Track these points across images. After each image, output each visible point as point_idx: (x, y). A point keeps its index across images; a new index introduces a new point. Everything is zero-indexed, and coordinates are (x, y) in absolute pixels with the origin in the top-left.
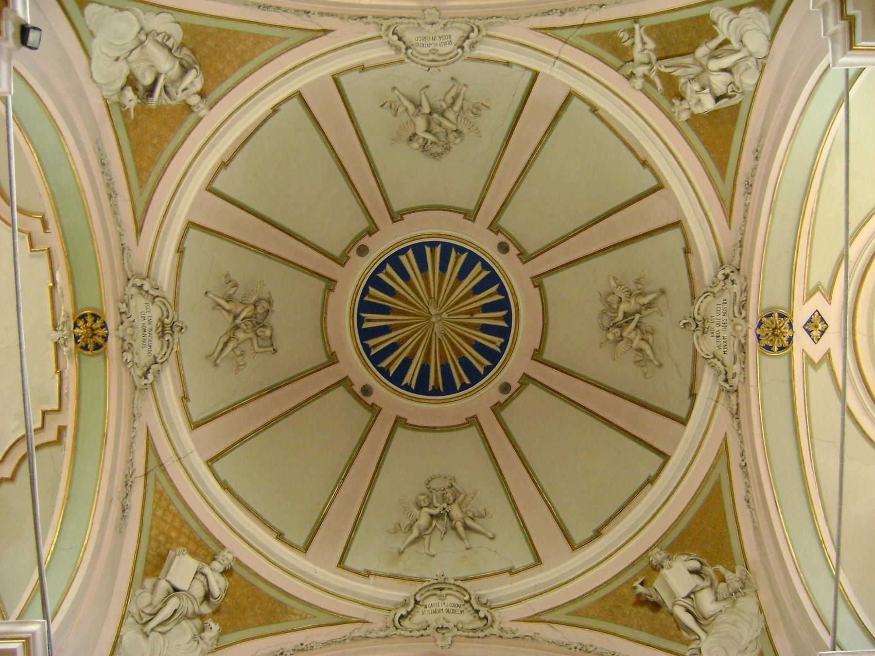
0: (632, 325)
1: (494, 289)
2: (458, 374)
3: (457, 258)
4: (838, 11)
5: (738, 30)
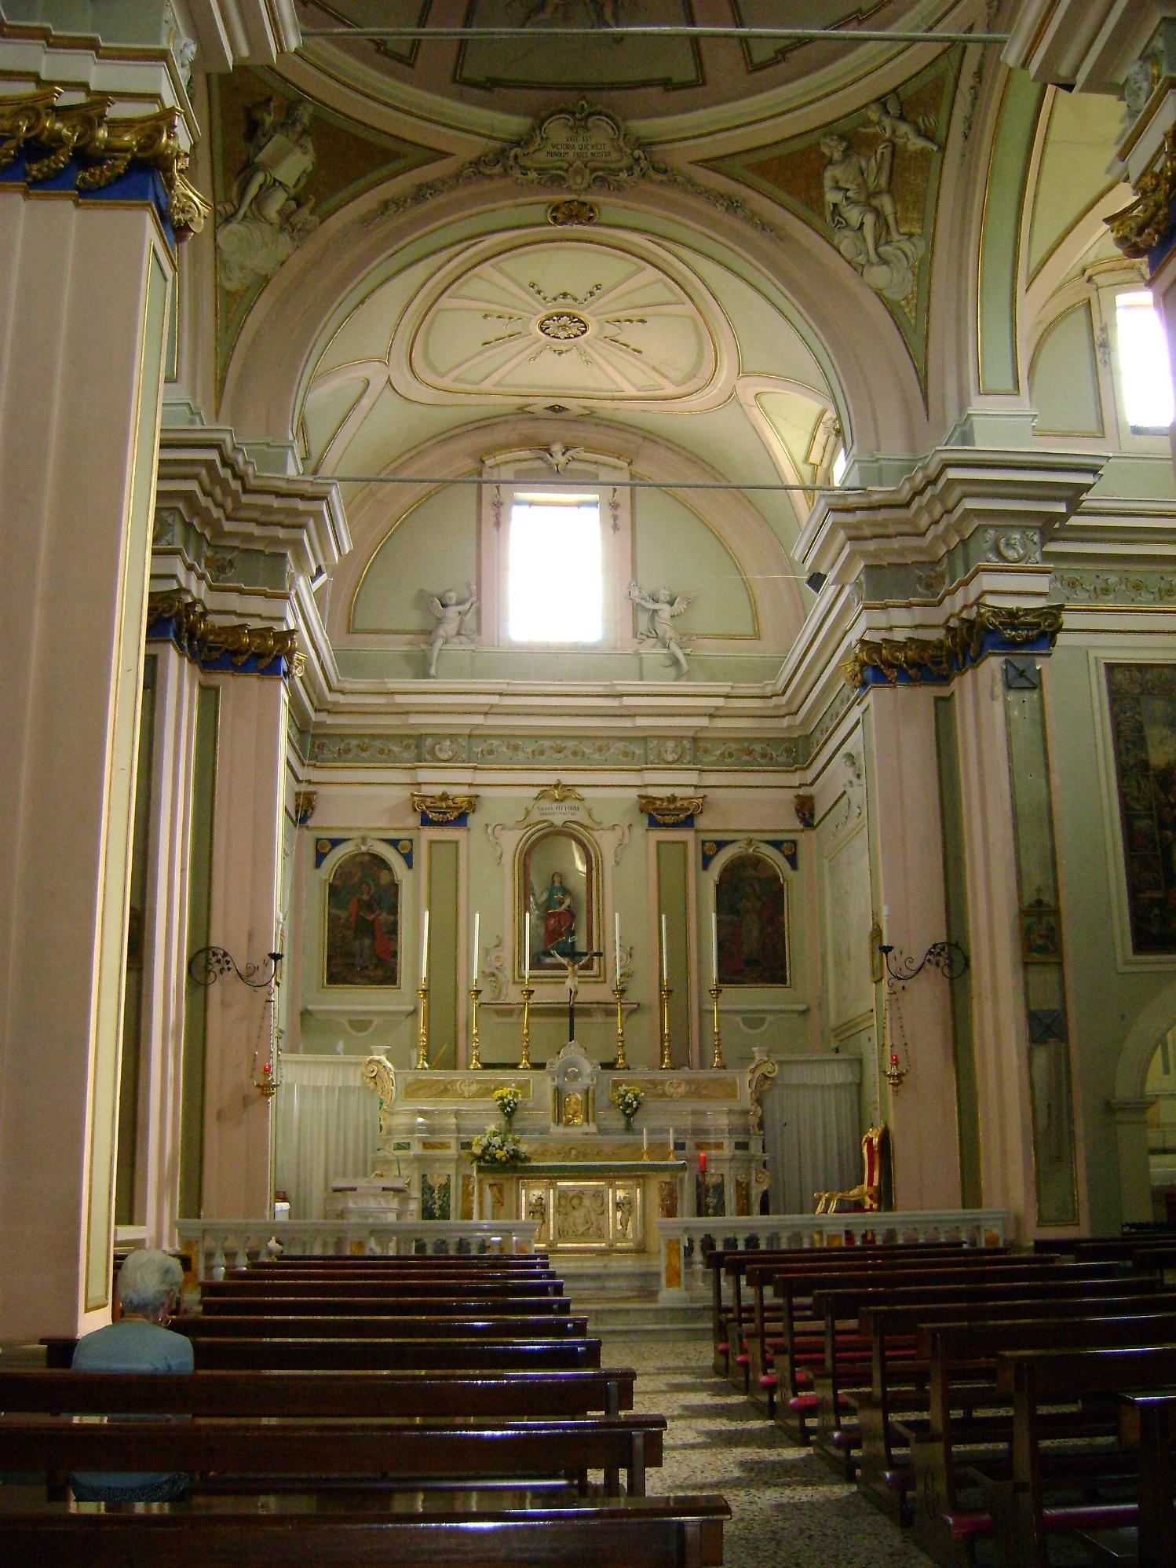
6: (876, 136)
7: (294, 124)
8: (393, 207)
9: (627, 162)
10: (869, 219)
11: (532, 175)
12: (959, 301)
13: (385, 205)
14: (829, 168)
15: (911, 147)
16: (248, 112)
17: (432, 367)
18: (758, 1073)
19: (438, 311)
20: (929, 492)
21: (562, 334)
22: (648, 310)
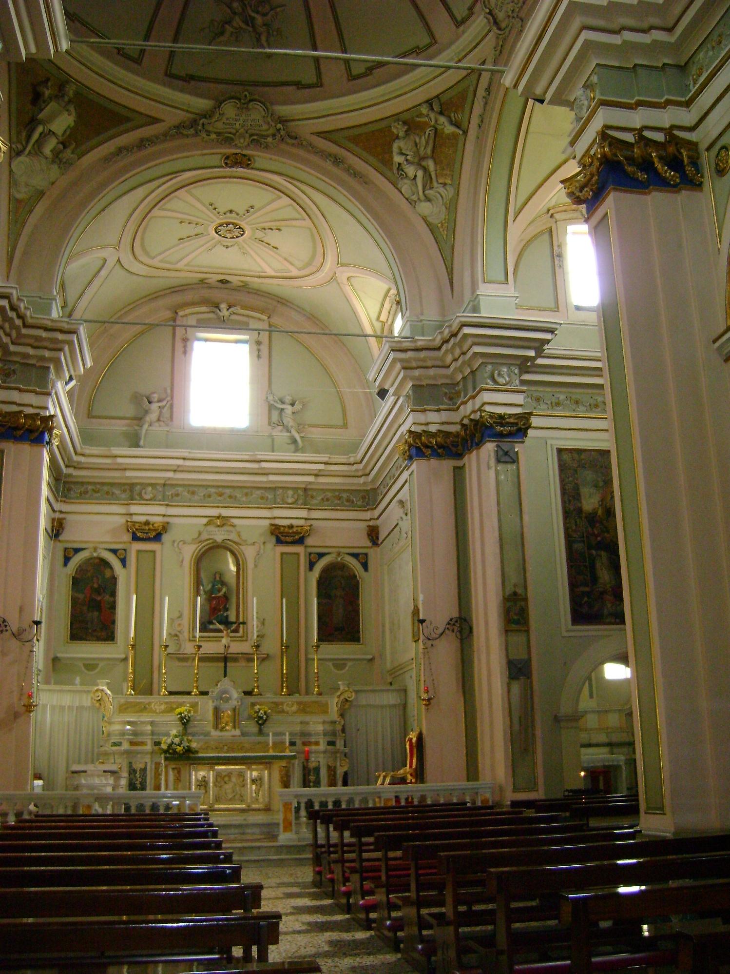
0: (243, 26)
6: (426, 124)
7: (63, 96)
8: (125, 152)
9: (271, 131)
10: (420, 174)
11: (213, 136)
12: (473, 229)
16: (34, 86)
17: (147, 254)
18: (342, 698)
21: (229, 235)
22: (283, 223)
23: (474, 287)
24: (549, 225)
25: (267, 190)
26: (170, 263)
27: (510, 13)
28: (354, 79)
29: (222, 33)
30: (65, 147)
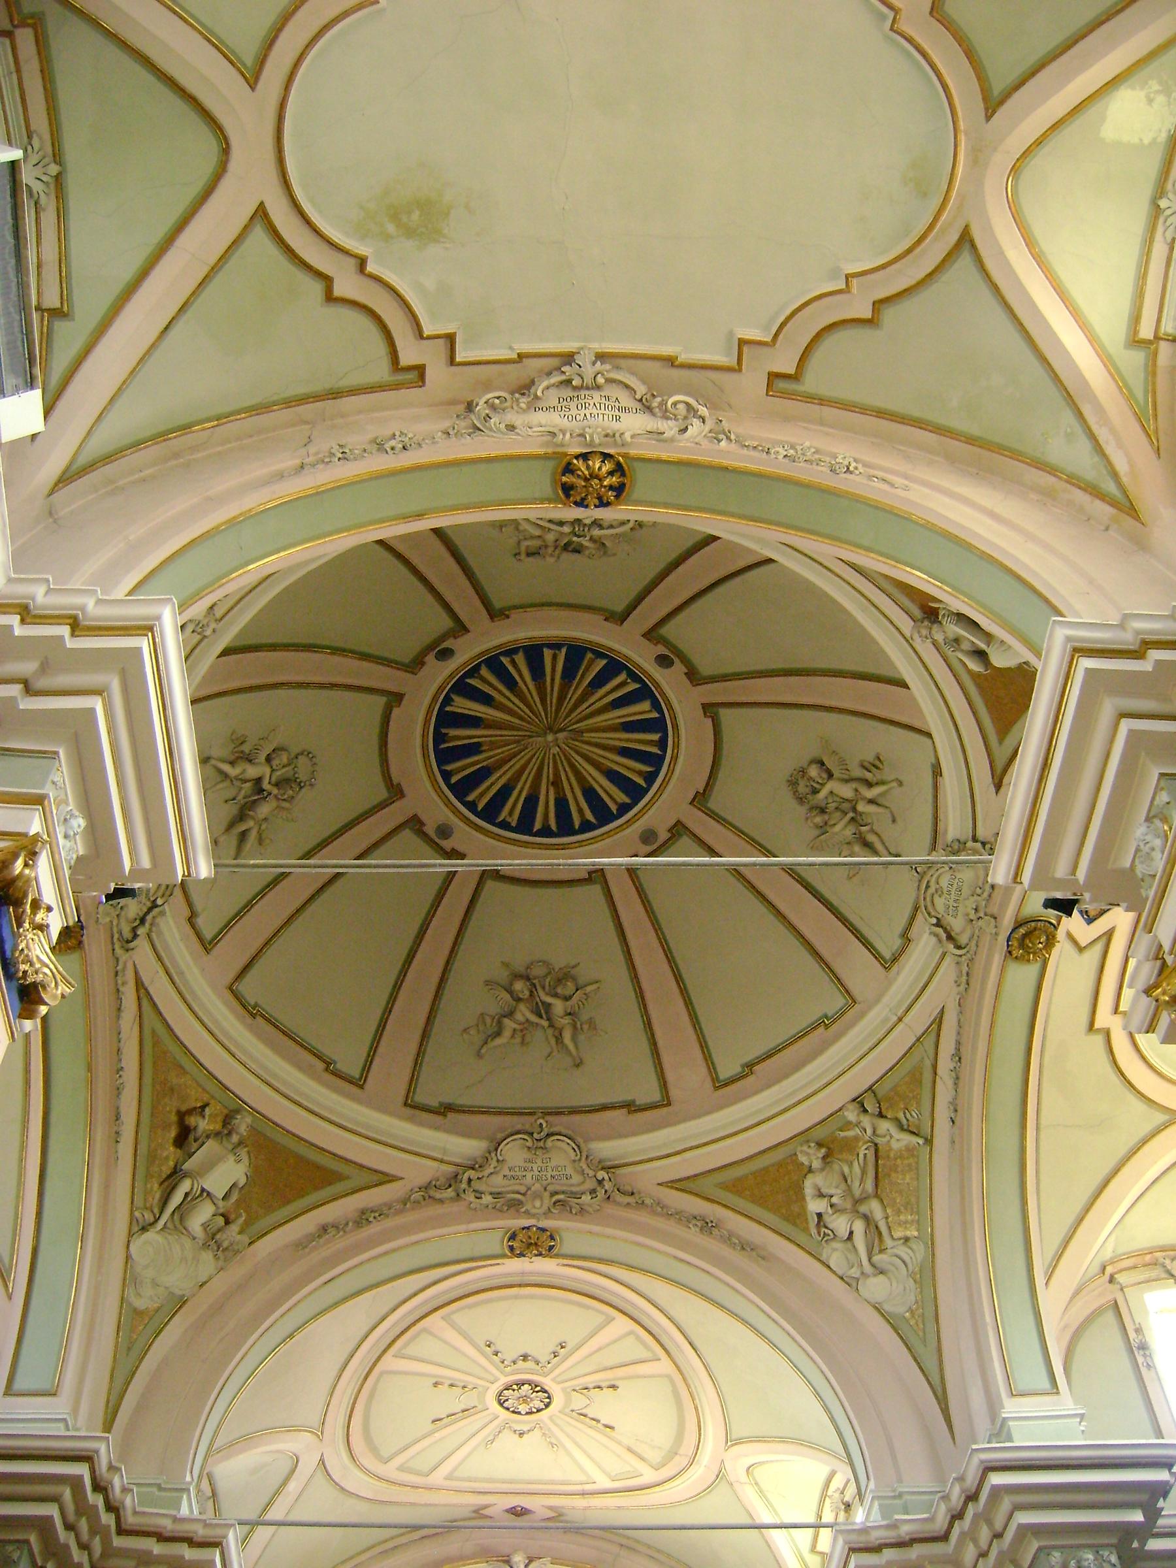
0: (533, 1018)
1: (590, 816)
2: (463, 768)
3: (640, 773)
4: (888, 1541)
5: (893, 1269)
6: (856, 1139)
7: (229, 1134)
8: (332, 1231)
9: (590, 1184)
10: (859, 1226)
11: (487, 1199)
12: (971, 1296)
13: (324, 1229)
14: (810, 1176)
15: (895, 1145)
16: (182, 1116)
17: (374, 1450)
19: (382, 1374)
20: (971, 1510)
21: (523, 1408)
22: (620, 1372)
23: (993, 1406)
24: (1110, 1297)
25: (588, 1307)
26: (418, 1473)
27: (972, 916)
28: (726, 1085)
29: (498, 1034)
30: (227, 1222)
